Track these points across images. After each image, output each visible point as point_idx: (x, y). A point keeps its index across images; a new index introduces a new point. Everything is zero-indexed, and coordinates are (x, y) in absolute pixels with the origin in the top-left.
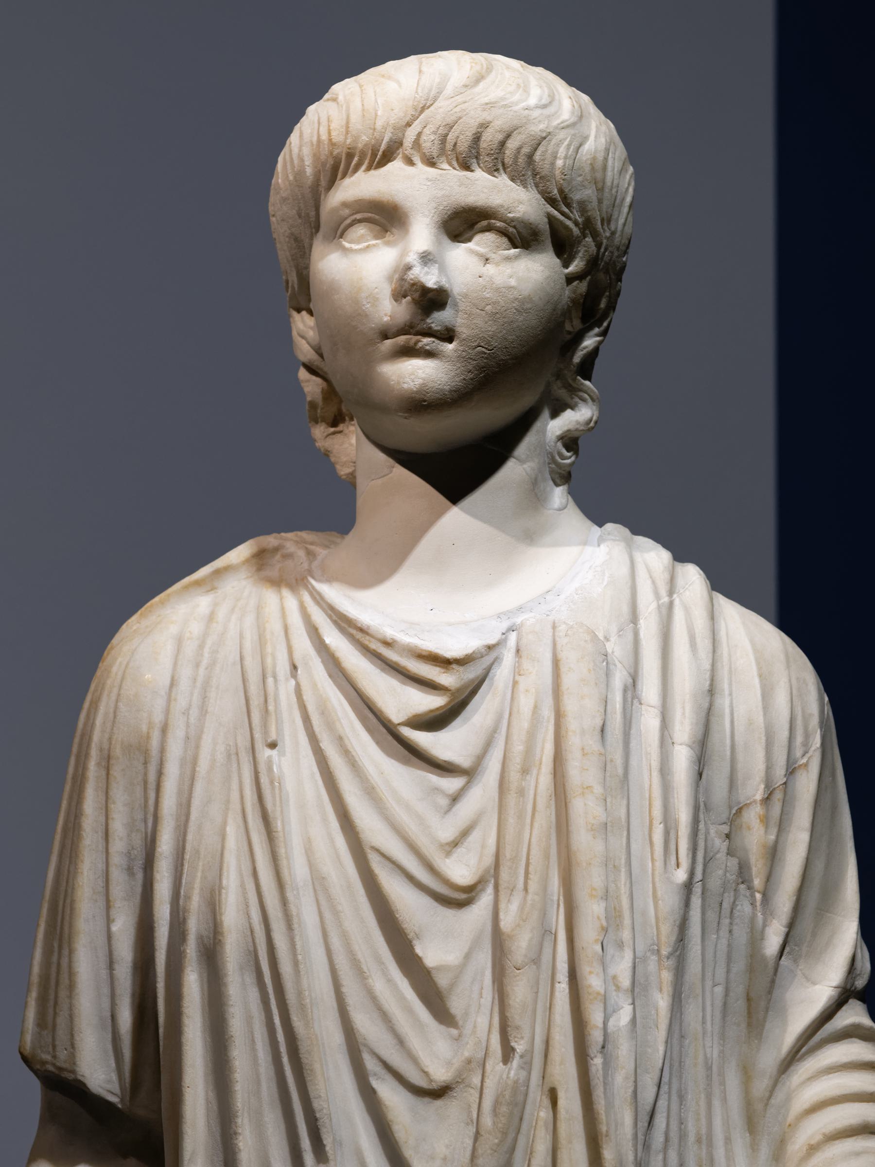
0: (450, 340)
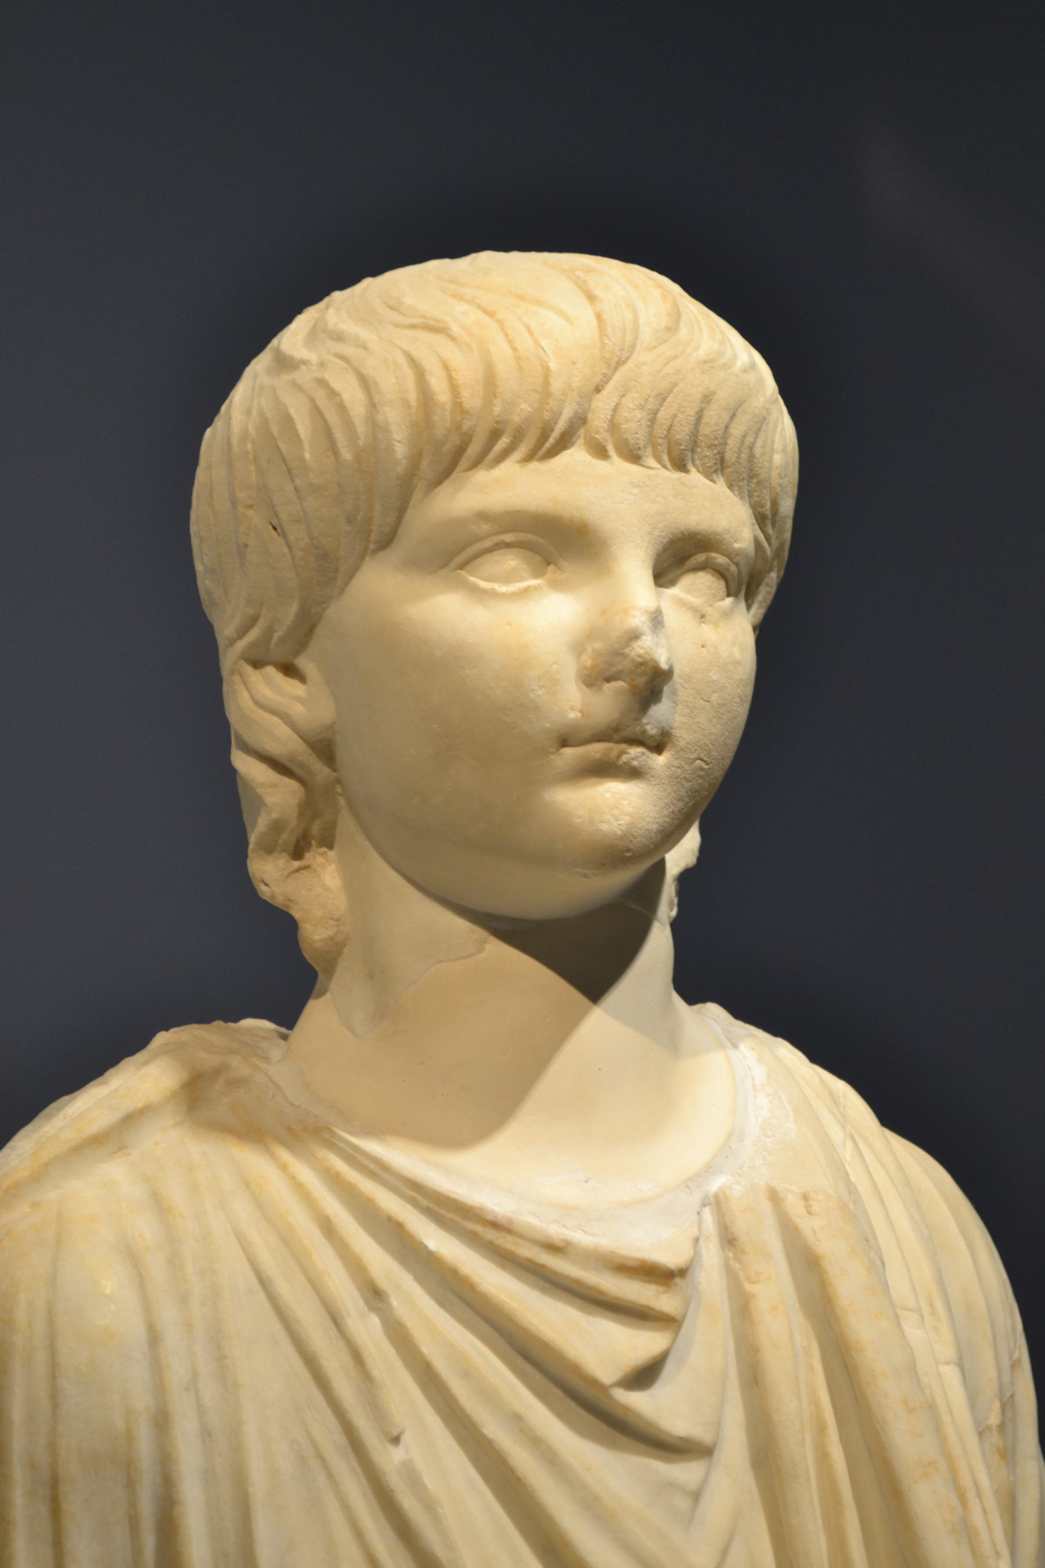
0: (658, 748)
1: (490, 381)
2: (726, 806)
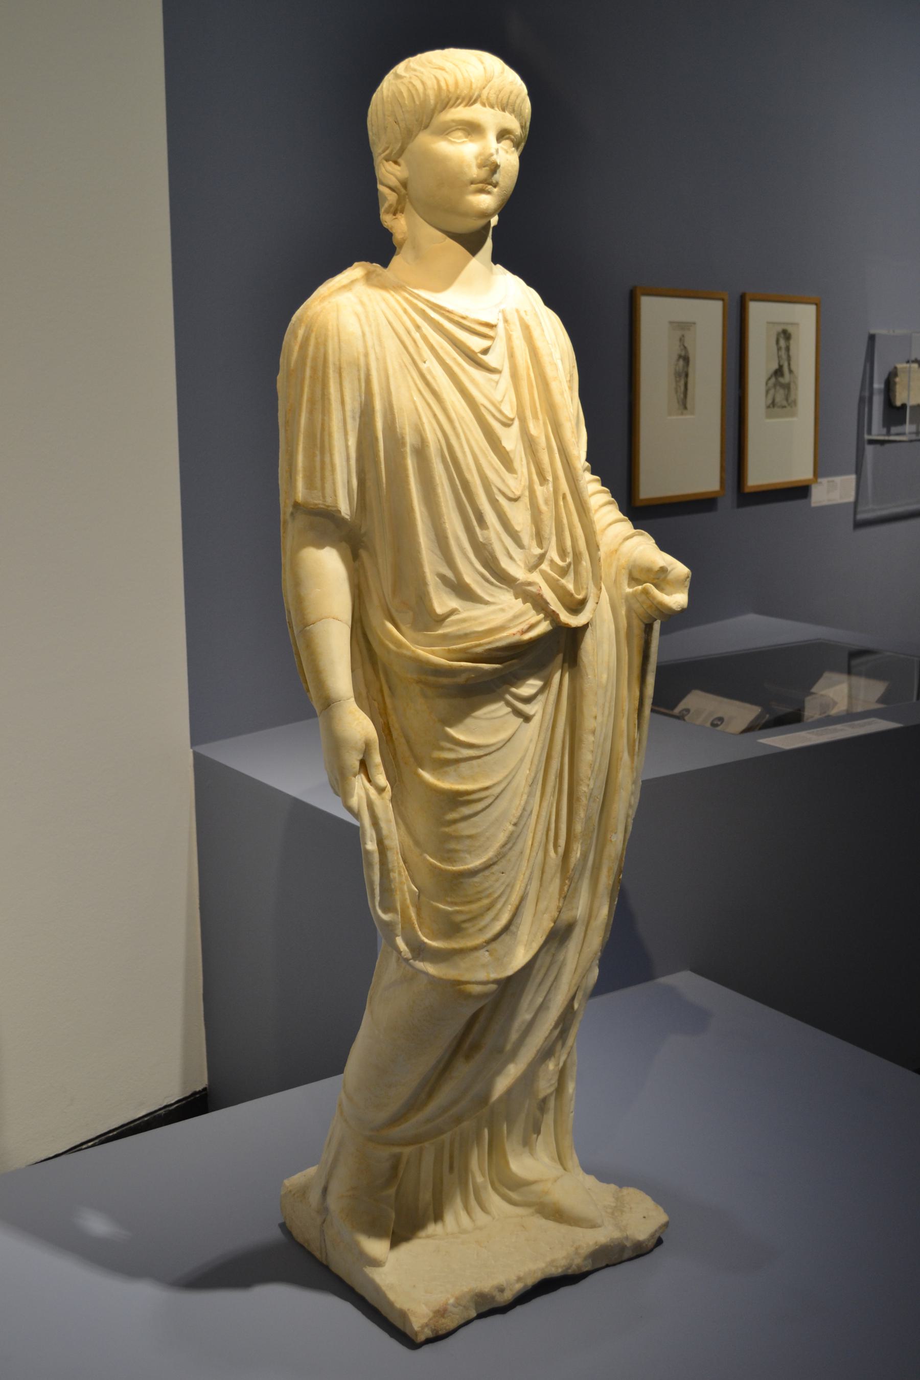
0: (495, 186)
1: (457, 84)
2: (507, 209)
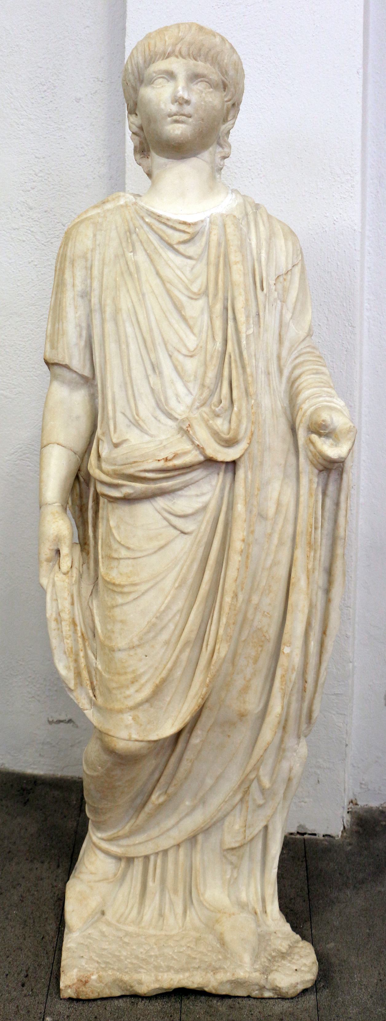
0: (190, 117)
